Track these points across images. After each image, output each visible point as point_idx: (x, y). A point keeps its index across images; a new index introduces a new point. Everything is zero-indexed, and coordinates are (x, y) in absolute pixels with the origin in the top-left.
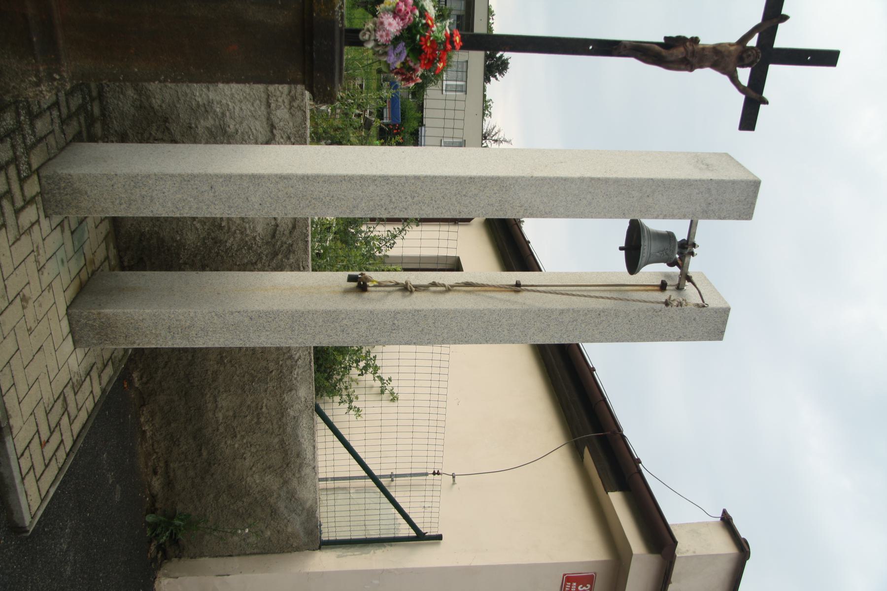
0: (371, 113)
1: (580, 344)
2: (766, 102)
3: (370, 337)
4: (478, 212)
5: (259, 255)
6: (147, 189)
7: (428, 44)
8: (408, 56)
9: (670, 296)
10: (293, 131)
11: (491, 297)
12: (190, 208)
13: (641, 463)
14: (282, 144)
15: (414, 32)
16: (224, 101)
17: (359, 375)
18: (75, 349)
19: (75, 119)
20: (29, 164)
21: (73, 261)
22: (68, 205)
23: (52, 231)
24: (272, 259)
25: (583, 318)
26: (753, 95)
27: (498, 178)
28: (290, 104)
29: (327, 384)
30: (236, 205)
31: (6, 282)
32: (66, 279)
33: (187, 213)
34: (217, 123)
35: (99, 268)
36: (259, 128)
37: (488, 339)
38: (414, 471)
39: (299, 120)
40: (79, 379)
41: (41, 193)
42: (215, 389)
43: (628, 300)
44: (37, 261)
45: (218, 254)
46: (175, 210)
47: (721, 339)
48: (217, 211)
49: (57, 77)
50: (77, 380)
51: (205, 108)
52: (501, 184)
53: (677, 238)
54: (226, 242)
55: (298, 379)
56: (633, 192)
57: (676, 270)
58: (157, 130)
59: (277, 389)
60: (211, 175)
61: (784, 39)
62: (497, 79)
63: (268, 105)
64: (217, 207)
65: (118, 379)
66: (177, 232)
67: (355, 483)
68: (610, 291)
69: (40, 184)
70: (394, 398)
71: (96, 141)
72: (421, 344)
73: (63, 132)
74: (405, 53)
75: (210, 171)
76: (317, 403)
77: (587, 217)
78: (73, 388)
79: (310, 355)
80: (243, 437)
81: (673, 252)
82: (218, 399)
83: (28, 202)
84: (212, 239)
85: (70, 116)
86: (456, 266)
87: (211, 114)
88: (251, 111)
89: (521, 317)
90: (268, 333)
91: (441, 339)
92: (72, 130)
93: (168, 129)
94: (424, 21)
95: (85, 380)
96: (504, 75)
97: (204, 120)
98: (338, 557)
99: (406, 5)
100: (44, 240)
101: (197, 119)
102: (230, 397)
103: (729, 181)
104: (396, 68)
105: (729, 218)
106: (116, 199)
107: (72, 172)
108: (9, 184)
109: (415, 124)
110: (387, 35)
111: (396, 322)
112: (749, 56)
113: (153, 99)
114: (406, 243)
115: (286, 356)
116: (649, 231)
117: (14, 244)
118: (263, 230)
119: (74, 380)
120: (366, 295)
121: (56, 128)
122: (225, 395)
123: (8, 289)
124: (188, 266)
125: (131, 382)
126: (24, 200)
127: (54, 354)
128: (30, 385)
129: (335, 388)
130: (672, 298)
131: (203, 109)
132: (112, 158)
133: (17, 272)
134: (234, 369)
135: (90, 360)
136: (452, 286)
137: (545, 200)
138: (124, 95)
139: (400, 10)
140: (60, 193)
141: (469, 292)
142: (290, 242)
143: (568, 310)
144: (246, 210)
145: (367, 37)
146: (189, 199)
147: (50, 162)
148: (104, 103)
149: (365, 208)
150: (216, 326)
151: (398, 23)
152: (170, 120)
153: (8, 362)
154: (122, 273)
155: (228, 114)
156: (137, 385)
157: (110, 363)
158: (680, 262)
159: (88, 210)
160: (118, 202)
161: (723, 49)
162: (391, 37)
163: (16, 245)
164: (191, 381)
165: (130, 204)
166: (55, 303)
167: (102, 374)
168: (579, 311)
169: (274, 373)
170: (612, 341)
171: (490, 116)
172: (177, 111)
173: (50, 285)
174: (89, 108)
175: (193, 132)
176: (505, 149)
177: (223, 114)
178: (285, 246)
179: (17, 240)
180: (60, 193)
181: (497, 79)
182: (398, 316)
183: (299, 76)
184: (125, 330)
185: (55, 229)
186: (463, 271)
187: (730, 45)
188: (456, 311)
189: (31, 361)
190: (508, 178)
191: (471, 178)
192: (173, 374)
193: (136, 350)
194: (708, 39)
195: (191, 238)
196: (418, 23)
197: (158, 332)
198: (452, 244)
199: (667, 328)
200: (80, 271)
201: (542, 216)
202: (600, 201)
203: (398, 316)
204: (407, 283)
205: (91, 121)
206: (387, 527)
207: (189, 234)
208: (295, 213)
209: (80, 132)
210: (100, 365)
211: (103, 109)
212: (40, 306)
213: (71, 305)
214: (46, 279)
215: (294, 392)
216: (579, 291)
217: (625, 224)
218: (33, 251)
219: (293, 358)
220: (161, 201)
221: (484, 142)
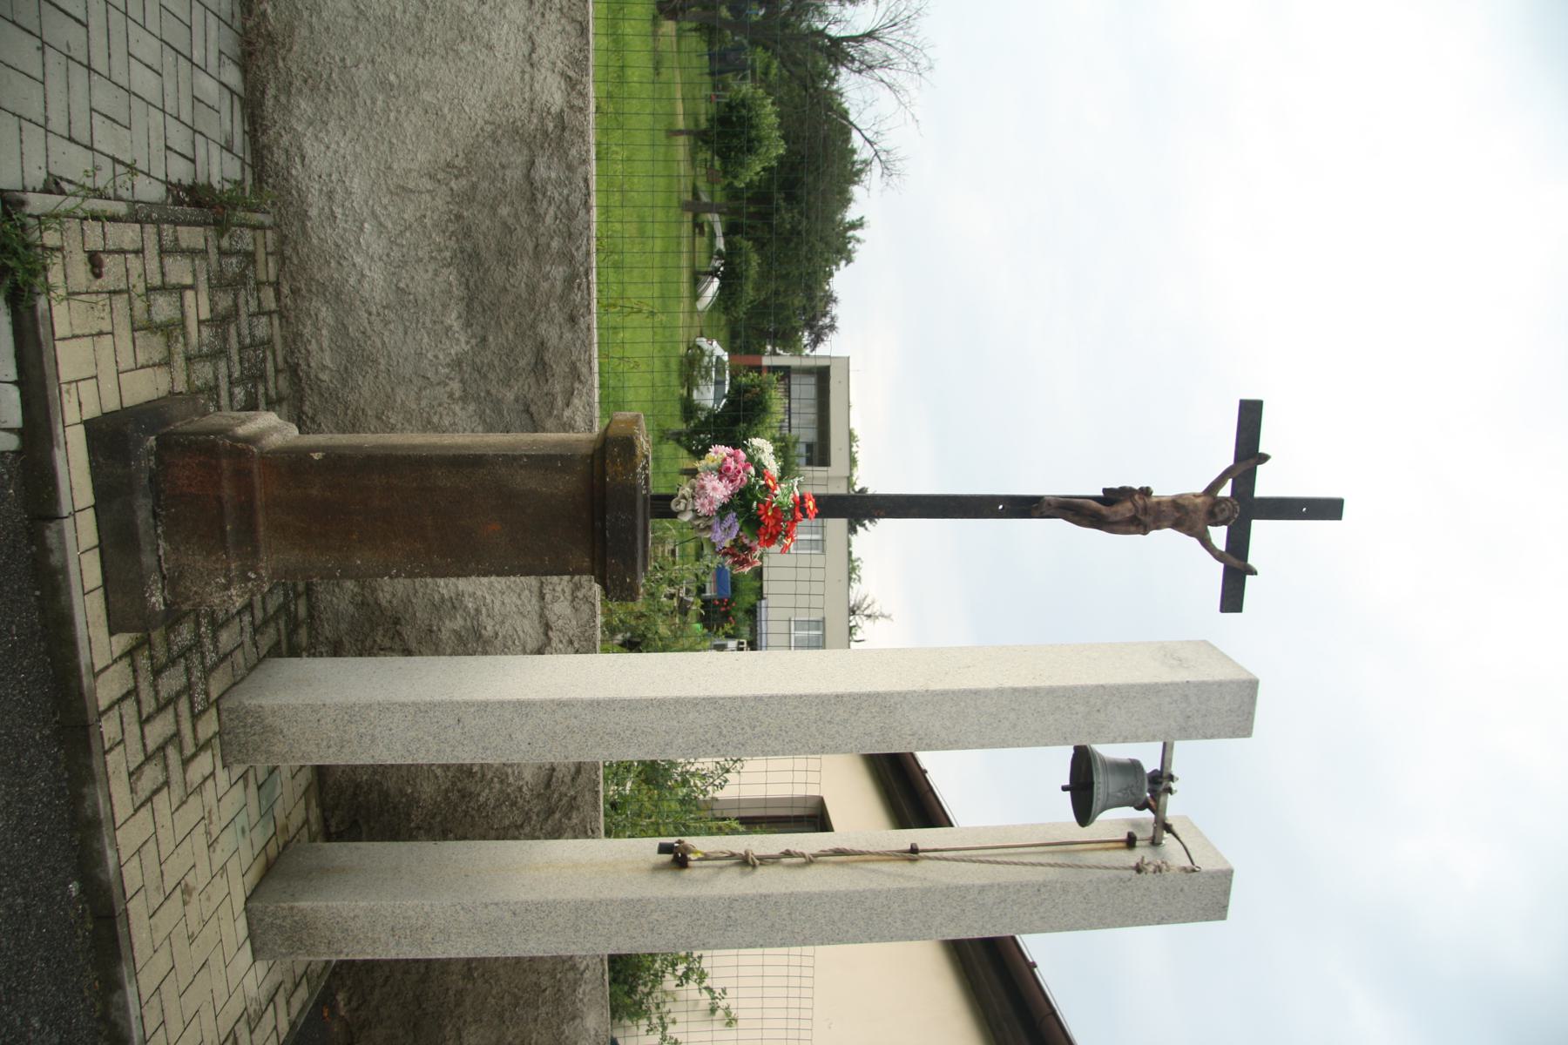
0: (688, 591)
2: (1253, 572)
3: (694, 938)
4: (850, 746)
5: (527, 813)
6: (366, 724)
7: (770, 514)
8: (741, 530)
9: (1143, 858)
10: (577, 631)
11: (874, 871)
12: (428, 751)
14: (561, 653)
15: (749, 496)
16: (479, 593)
17: (677, 985)
18: (254, 962)
19: (273, 624)
20: (207, 694)
21: (259, 828)
22: (254, 750)
23: (231, 786)
24: (546, 819)
25: (1015, 897)
26: (1235, 562)
27: (878, 695)
28: (572, 594)
29: (628, 1001)
30: (494, 745)
31: (163, 867)
32: (247, 856)
33: (423, 759)
34: (469, 623)
35: (294, 837)
36: (527, 628)
37: (872, 935)
39: (585, 617)
40: (258, 1008)
41: (219, 734)
42: (459, 1018)
43: (1080, 867)
44: (208, 833)
45: (466, 813)
46: (406, 754)
47: (1223, 917)
48: (466, 756)
49: (253, 576)
50: (255, 1011)
51: (453, 603)
52: (881, 702)
54: (479, 795)
55: (585, 1000)
56: (1076, 706)
57: (1147, 814)
58: (384, 636)
59: (553, 1016)
60: (458, 703)
61: (1267, 484)
63: (542, 597)
64: (467, 749)
65: (316, 1005)
66: (408, 781)
68: (1053, 853)
69: (219, 720)
70: (731, 1021)
71: (299, 655)
72: (771, 945)
73: (255, 644)
74: (737, 526)
75: (457, 697)
76: (614, 1036)
77: (1012, 746)
78: (249, 1024)
79: (603, 964)
81: (1142, 790)
82: (464, 1034)
83: (201, 748)
84: (459, 791)
85: (266, 622)
86: (816, 818)
87: (461, 612)
88: (516, 606)
89: (920, 900)
90: (540, 935)
91: (800, 938)
92: (266, 642)
93: (400, 634)
94: (762, 482)
95: (266, 1009)
97: (450, 620)
99: (736, 461)
100: (219, 800)
101: (440, 619)
102: (482, 1030)
103: (1214, 683)
104: (724, 548)
105: (1219, 736)
106: (322, 740)
107: (263, 702)
108: (177, 722)
109: (752, 598)
110: (711, 503)
111: (732, 914)
112: (1224, 510)
113: (379, 592)
114: (745, 778)
115: (567, 966)
116: (1103, 761)
117: (177, 809)
118: (533, 776)
119: (251, 1010)
120: (686, 872)
121: (247, 639)
122: (473, 1028)
123: (165, 878)
124: (422, 832)
125: (333, 1008)
126: (197, 745)
127: (223, 972)
128: (187, 1023)
129: (641, 1008)
130: (1146, 861)
131: (449, 605)
132: (319, 680)
133: (179, 849)
134: (487, 986)
135: (276, 977)
136: (815, 856)
137: (948, 724)
138: (341, 588)
139: (728, 469)
140: (245, 733)
141: (842, 863)
142: (573, 793)
143: (992, 886)
144: (508, 752)
145: (682, 507)
146: (426, 738)
147: (234, 688)
148: (314, 600)
149: (683, 746)
150: (462, 925)
151: (726, 487)
152: (403, 622)
153: (158, 988)
154: (327, 845)
155: (484, 611)
156: (342, 1013)
157: (304, 980)
158: (1152, 803)
159: (283, 756)
160: (325, 743)
161: (1186, 502)
162: (716, 506)
163: (180, 810)
164: (424, 1006)
165: (342, 747)
166: (229, 893)
167: (292, 999)
168: (1007, 887)
169: (547, 992)
170: (1060, 930)
171: (859, 580)
172: (413, 608)
173: (224, 868)
174: (293, 608)
175: (434, 637)
176: (885, 650)
177: (478, 611)
178: (565, 800)
179: (183, 803)
180: (245, 733)
182: (736, 905)
183: (587, 563)
184: (328, 933)
185: (235, 783)
186: (832, 830)
187: (1196, 496)
188: (821, 895)
189: (191, 983)
190: (891, 695)
191: (837, 696)
192: (396, 995)
193: (342, 963)
194: (1164, 488)
195: (427, 790)
196: (754, 485)
197: (376, 936)
198: (813, 777)
199: (1141, 905)
200: (267, 843)
201: (945, 748)
202: (1029, 721)
203: (736, 905)
204: (747, 854)
205: (294, 625)
207: (425, 785)
208: (580, 756)
209: (278, 643)
210: (289, 985)
211: (311, 608)
212: (208, 899)
213: (251, 895)
214: (219, 857)
215: (578, 1021)
216: (1006, 855)
217: (1068, 752)
218: (203, 818)
219: (578, 969)
220: (386, 741)
221: (851, 618)
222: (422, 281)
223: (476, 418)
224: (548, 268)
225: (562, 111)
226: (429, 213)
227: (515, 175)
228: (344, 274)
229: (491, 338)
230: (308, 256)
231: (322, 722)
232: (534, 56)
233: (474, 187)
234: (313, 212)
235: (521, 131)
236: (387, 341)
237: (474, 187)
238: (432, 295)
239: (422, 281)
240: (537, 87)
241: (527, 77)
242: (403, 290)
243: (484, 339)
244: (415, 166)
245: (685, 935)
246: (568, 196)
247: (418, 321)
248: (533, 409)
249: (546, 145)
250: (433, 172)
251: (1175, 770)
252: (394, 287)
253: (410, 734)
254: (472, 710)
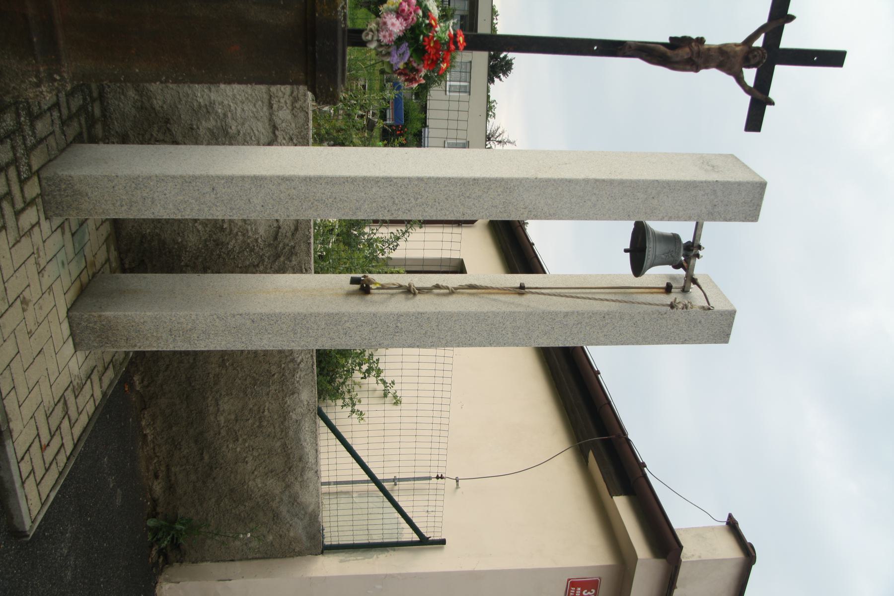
0: (374, 114)
2: (772, 103)
3: (373, 340)
4: (482, 214)
5: (261, 257)
6: (148, 190)
7: (432, 45)
8: (411, 56)
9: (676, 299)
10: (296, 132)
11: (495, 300)
12: (192, 210)
13: (646, 467)
14: (284, 145)
15: (417, 32)
16: (226, 102)
17: (362, 378)
18: (76, 352)
19: (76, 120)
20: (30, 166)
21: (74, 263)
22: (68, 207)
23: (53, 233)
24: (274, 261)
25: (588, 321)
26: (759, 95)
27: (502, 179)
28: (292, 105)
29: (330, 387)
30: (238, 206)
31: (6, 285)
32: (67, 282)
33: (188, 215)
34: (219, 124)
35: (100, 270)
36: (261, 129)
37: (492, 342)
38: (417, 475)
39: (301, 121)
40: (79, 382)
41: (41, 195)
42: (217, 392)
43: (633, 303)
44: (37, 264)
45: (219, 256)
46: (177, 212)
47: (727, 342)
48: (219, 213)
49: (58, 78)
50: (78, 383)
51: (207, 109)
52: (505, 185)
53: (682, 240)
54: (228, 244)
55: (301, 382)
56: (638, 194)
57: (681, 272)
58: (158, 131)
59: (279, 392)
60: (212, 176)
61: (790, 39)
62: (501, 80)
63: (271, 106)
64: (219, 209)
65: (119, 382)
66: (179, 234)
67: (357, 487)
68: (615, 293)
69: (40, 186)
70: (397, 402)
71: (97, 143)
72: (424, 347)
73: (63, 133)
74: (409, 53)
75: (212, 172)
76: (320, 406)
77: (592, 219)
78: (74, 392)
79: (312, 358)
80: (245, 441)
81: (678, 254)
82: (220, 403)
83: (28, 204)
84: (214, 241)
85: (70, 117)
86: (459, 268)
87: (213, 115)
88: (253, 112)
89: (525, 320)
90: (270, 336)
91: (444, 342)
92: (72, 131)
93: (169, 130)
94: (427, 22)
95: (85, 383)
96: (508, 76)
97: (206, 121)
98: (341, 561)
99: (409, 5)
100: (44, 242)
101: (199, 120)
102: (232, 400)
103: (735, 183)
104: (399, 69)
105: (735, 220)
106: (117, 201)
107: (72, 174)
108: (9, 185)
109: (418, 125)
110: (390, 35)
111: (399, 325)
112: (755, 56)
113: (154, 100)
114: (409, 245)
115: (288, 359)
116: (654, 233)
117: (14, 246)
118: (265, 231)
119: (75, 383)
120: (369, 297)
121: (57, 129)
122: (226, 399)
123: (8, 292)
124: (189, 268)
125: (132, 386)
126: (25, 202)
127: (54, 357)
128: (31, 389)
129: (338, 392)
130: (678, 301)
131: (205, 110)
132: (113, 159)
133: (17, 274)
134: (236, 372)
135: (91, 363)
136: (456, 289)
137: (549, 202)
138: (125, 96)
139: (403, 10)
140: (60, 195)
141: (473, 294)
142: (293, 244)
143: (573, 313)
144: (248, 211)
145: (370, 37)
146: (190, 200)
147: (51, 164)
148: (105, 104)
149: (368, 210)
150: (217, 329)
151: (401, 24)
152: (172, 121)
153: (9, 365)
154: (123, 275)
155: (229, 115)
156: (138, 389)
157: (111, 366)
158: (685, 264)
159: (89, 212)
160: (118, 203)
161: (729, 50)
162: (394, 37)
163: (16, 247)
164: (193, 384)
165: (131, 206)
166: (55, 305)
167: (103, 378)
168: (583, 314)
169: (276, 376)
170: (617, 344)
171: (494, 116)
172: (179, 112)
173: (50, 288)
174: (90, 109)
175: (194, 133)
176: (509, 150)
177: (225, 115)
178: (287, 248)
179: (18, 242)
180: (60, 195)
181: (501, 80)
182: (401, 319)
183: (302, 76)
184: (126, 333)
185: (55, 230)
186: (466, 273)
187: (736, 45)
188: (459, 314)
189: (31, 364)
190: (512, 180)
191: (474, 179)
192: (174, 377)
193: (137, 353)
194: (713, 40)
195: (192, 240)
196: (421, 24)
197: (159, 335)
198: (455, 246)
199: (672, 330)
200: (81, 273)
201: (546, 218)
202: (605, 203)
203: (401, 319)
204: (410, 286)
205: (91, 122)
206: (390, 531)
207: (190, 236)
208: (297, 215)
209: (81, 134)
210: (100, 368)
211: (104, 110)
212: (41, 308)
213: (71, 307)
214: (47, 281)
215: (296, 395)
216: (583, 293)
217: (630, 226)
218: (33, 253)
219: (296, 361)
220: (162, 202)
221: (487, 143)
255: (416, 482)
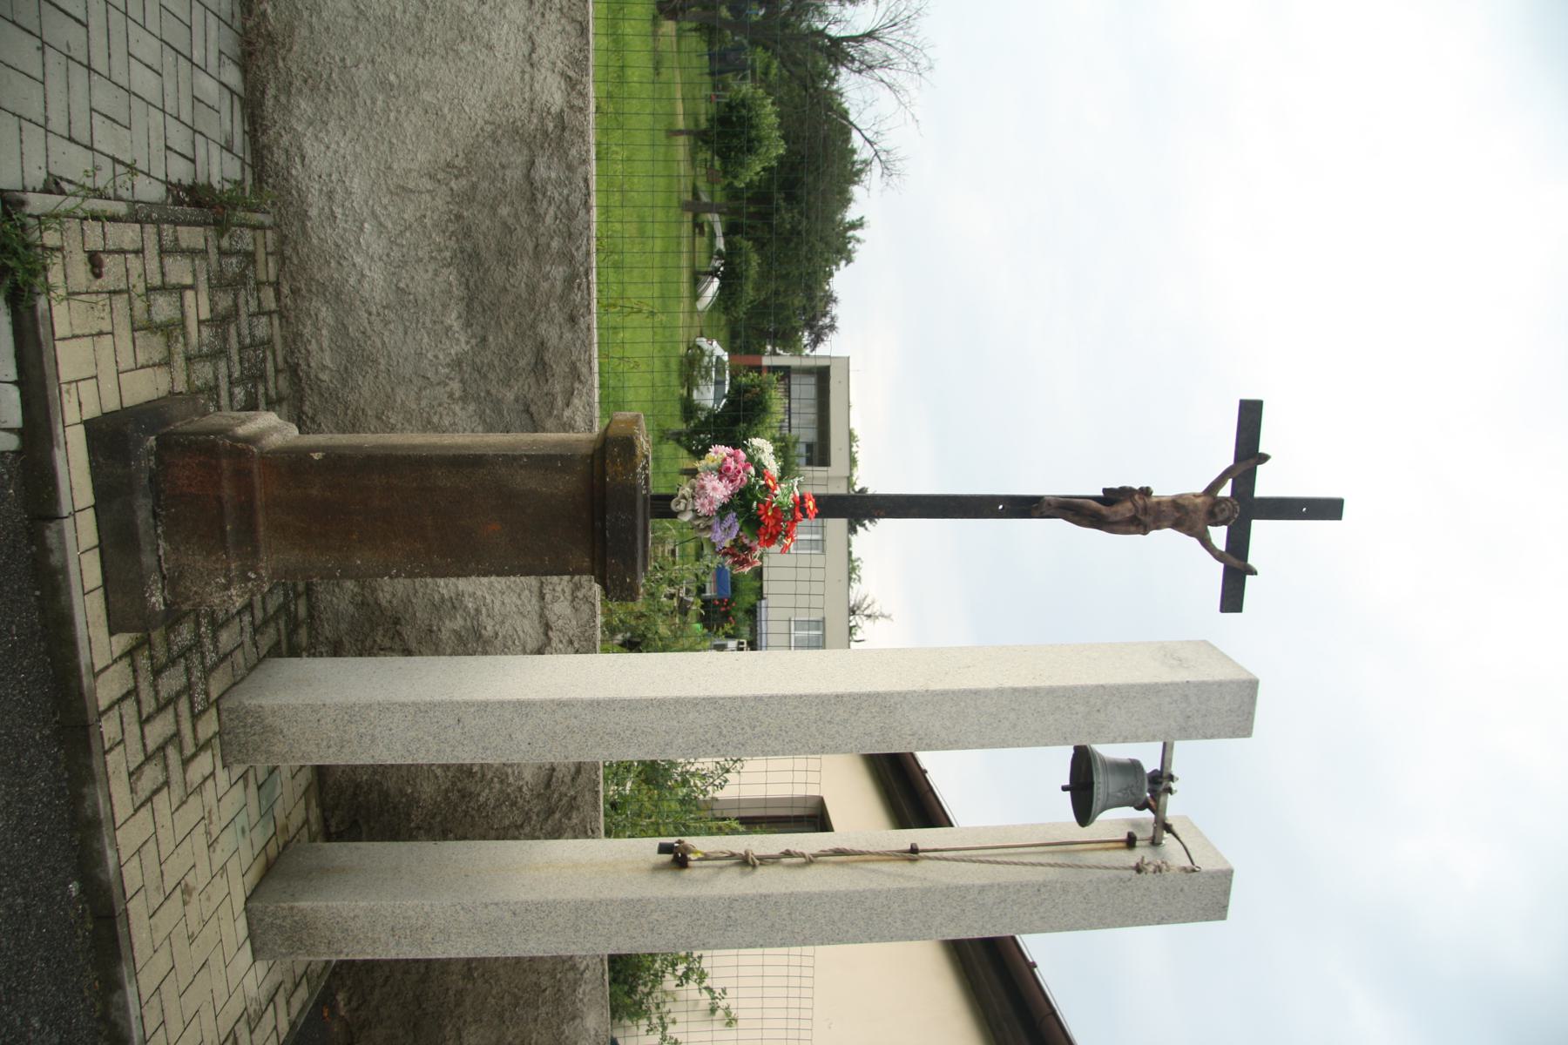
0: (688, 591)
1: (1017, 937)
2: (1253, 572)
3: (694, 938)
4: (850, 746)
5: (527, 813)
6: (366, 724)
7: (770, 514)
8: (741, 530)
9: (1143, 858)
10: (577, 631)
11: (874, 871)
12: (428, 751)
14: (561, 653)
15: (749, 496)
16: (479, 593)
17: (677, 985)
18: (254, 962)
19: (273, 624)
20: (207, 694)
21: (259, 828)
22: (254, 750)
23: (231, 786)
24: (546, 819)
25: (1015, 897)
26: (1235, 562)
27: (878, 695)
28: (572, 594)
29: (628, 1001)
30: (494, 745)
31: (163, 867)
32: (247, 856)
33: (423, 759)
34: (469, 623)
35: (294, 837)
36: (527, 628)
37: (872, 935)
39: (585, 617)
40: (258, 1008)
41: (219, 734)
42: (459, 1018)
43: (1080, 867)
44: (208, 833)
45: (466, 813)
46: (406, 754)
47: (1223, 917)
48: (466, 756)
49: (253, 576)
50: (255, 1011)
51: (453, 603)
52: (881, 702)
54: (479, 795)
55: (585, 1000)
56: (1076, 706)
57: (1147, 814)
58: (384, 636)
59: (553, 1016)
60: (458, 703)
61: (1267, 484)
63: (542, 597)
64: (467, 749)
65: (316, 1005)
66: (408, 781)
68: (1053, 853)
69: (219, 720)
70: (731, 1021)
71: (299, 655)
72: (771, 945)
73: (255, 644)
74: (737, 526)
75: (457, 697)
76: (614, 1036)
77: (1012, 746)
78: (249, 1024)
79: (603, 964)
81: (1142, 790)
82: (464, 1034)
83: (201, 748)
84: (459, 791)
85: (266, 622)
86: (816, 818)
87: (461, 612)
88: (516, 606)
89: (920, 900)
90: (540, 935)
91: (800, 938)
92: (266, 642)
93: (400, 634)
94: (762, 482)
95: (266, 1009)
97: (450, 620)
99: (736, 461)
100: (219, 800)
101: (440, 619)
102: (482, 1030)
103: (1214, 683)
104: (724, 548)
105: (1219, 736)
106: (322, 740)
107: (263, 702)
108: (177, 722)
109: (752, 598)
110: (711, 503)
111: (732, 914)
112: (1224, 510)
113: (379, 592)
114: (745, 778)
115: (567, 966)
116: (1103, 761)
117: (177, 809)
118: (533, 776)
119: (251, 1010)
120: (686, 872)
121: (247, 639)
122: (473, 1028)
123: (165, 878)
124: (422, 832)
125: (333, 1008)
126: (197, 745)
127: (223, 972)
128: (187, 1023)
129: (641, 1008)
130: (1146, 861)
131: (449, 605)
132: (319, 680)
133: (179, 849)
134: (487, 986)
135: (276, 977)
136: (815, 856)
137: (948, 724)
138: (341, 588)
139: (728, 469)
140: (245, 733)
141: (842, 863)
142: (573, 793)
143: (992, 886)
144: (508, 752)
145: (682, 507)
146: (426, 738)
147: (234, 688)
148: (314, 600)
149: (683, 746)
150: (462, 925)
151: (726, 487)
152: (403, 622)
153: (158, 988)
154: (327, 845)
155: (484, 611)
156: (342, 1013)
157: (304, 980)
158: (1152, 803)
159: (283, 756)
160: (325, 743)
161: (1186, 502)
162: (716, 506)
163: (180, 810)
164: (424, 1006)
165: (342, 747)
166: (229, 893)
167: (292, 999)
168: (1007, 887)
169: (547, 992)
170: (1060, 930)
171: (859, 580)
172: (413, 608)
173: (224, 868)
174: (293, 608)
175: (434, 637)
176: (885, 650)
177: (478, 611)
178: (565, 800)
179: (183, 803)
180: (245, 733)
182: (736, 905)
183: (587, 563)
184: (328, 933)
185: (235, 783)
186: (832, 830)
187: (1196, 496)
188: (821, 895)
189: (191, 983)
190: (891, 695)
191: (837, 696)
192: (396, 995)
193: (342, 963)
194: (1164, 488)
195: (427, 790)
196: (754, 485)
197: (376, 936)
198: (813, 777)
199: (1141, 905)
200: (267, 843)
201: (945, 748)
202: (1029, 721)
203: (736, 905)
204: (747, 854)
205: (294, 625)
207: (425, 785)
208: (580, 756)
209: (278, 643)
210: (289, 985)
211: (311, 608)
212: (208, 899)
213: (251, 895)
214: (219, 857)
215: (578, 1021)
216: (1006, 855)
217: (1068, 752)
218: (203, 818)
219: (578, 969)
220: (386, 741)
221: (851, 618)
222: (422, 281)
223: (476, 418)
224: (548, 268)
225: (562, 111)
226: (429, 213)
227: (515, 175)
228: (344, 274)
229: (491, 338)
230: (308, 256)
231: (322, 722)
232: (534, 56)
233: (474, 187)
234: (313, 212)
235: (521, 131)
236: (387, 341)
237: (474, 187)
238: (432, 295)
239: (422, 281)
240: (537, 87)
241: (527, 77)
242: (403, 290)
243: (484, 339)
244: (415, 166)
245: (685, 935)
246: (568, 196)
247: (418, 321)
248: (533, 409)
249: (546, 145)
250: (433, 172)
251: (1175, 770)
252: (394, 287)
253: (410, 734)
254: (472, 710)
255: (697, 250)
